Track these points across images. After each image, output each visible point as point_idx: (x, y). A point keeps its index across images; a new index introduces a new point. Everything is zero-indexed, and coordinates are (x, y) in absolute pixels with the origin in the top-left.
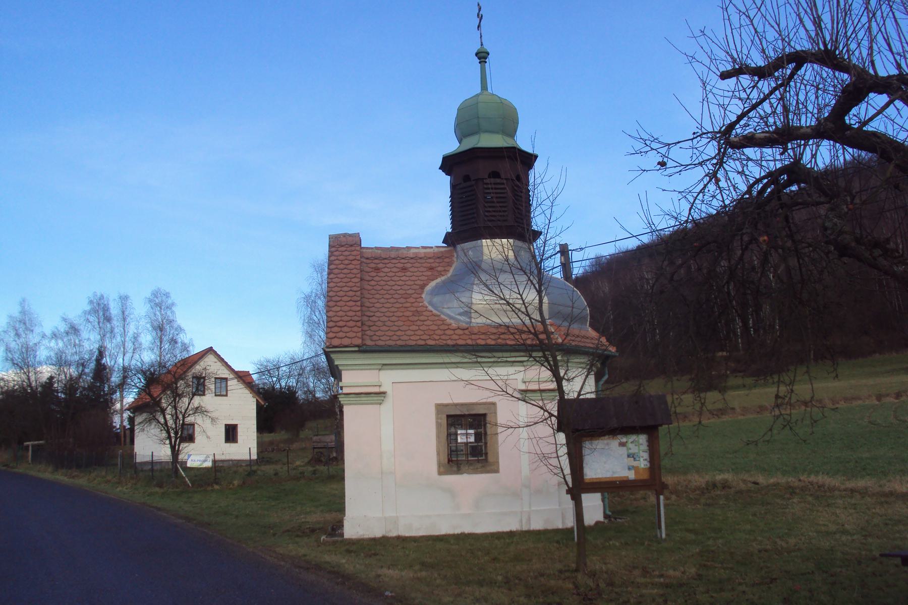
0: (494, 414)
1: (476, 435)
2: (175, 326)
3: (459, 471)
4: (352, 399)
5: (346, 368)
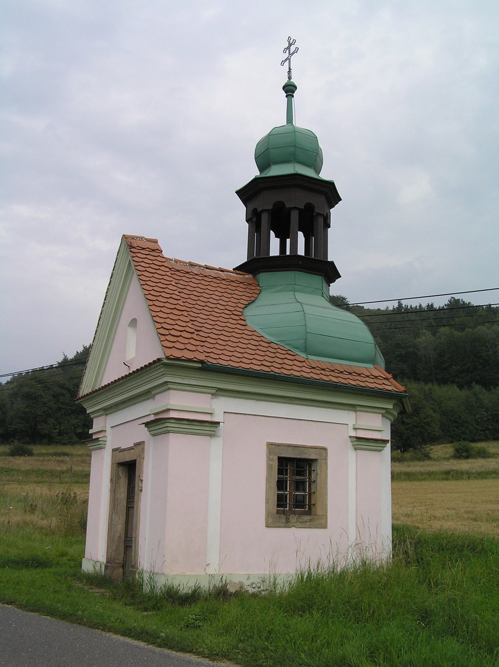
0: (324, 460)
2: (229, 593)
3: (287, 524)
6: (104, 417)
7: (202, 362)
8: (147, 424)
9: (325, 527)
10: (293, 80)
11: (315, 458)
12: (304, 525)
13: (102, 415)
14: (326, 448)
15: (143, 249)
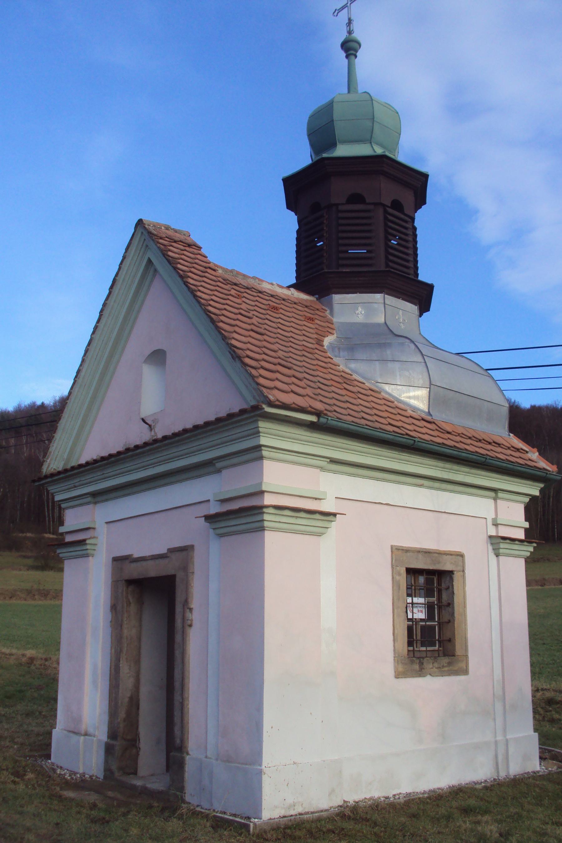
1: (430, 608)
3: (421, 673)
4: (286, 518)
5: (273, 455)
6: (91, 506)
7: (318, 414)
8: (209, 518)
9: (465, 672)
10: (357, 35)
11: (450, 570)
12: (442, 672)
13: (88, 503)
14: (463, 553)
15: (175, 242)
